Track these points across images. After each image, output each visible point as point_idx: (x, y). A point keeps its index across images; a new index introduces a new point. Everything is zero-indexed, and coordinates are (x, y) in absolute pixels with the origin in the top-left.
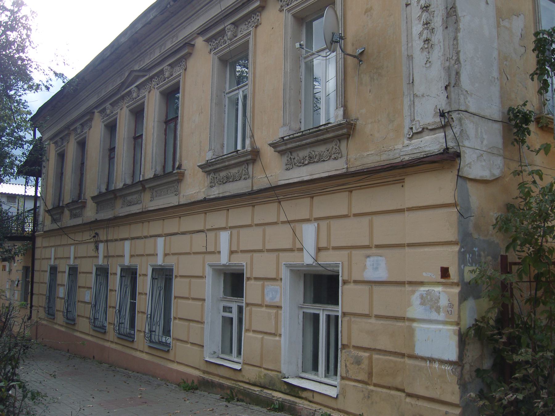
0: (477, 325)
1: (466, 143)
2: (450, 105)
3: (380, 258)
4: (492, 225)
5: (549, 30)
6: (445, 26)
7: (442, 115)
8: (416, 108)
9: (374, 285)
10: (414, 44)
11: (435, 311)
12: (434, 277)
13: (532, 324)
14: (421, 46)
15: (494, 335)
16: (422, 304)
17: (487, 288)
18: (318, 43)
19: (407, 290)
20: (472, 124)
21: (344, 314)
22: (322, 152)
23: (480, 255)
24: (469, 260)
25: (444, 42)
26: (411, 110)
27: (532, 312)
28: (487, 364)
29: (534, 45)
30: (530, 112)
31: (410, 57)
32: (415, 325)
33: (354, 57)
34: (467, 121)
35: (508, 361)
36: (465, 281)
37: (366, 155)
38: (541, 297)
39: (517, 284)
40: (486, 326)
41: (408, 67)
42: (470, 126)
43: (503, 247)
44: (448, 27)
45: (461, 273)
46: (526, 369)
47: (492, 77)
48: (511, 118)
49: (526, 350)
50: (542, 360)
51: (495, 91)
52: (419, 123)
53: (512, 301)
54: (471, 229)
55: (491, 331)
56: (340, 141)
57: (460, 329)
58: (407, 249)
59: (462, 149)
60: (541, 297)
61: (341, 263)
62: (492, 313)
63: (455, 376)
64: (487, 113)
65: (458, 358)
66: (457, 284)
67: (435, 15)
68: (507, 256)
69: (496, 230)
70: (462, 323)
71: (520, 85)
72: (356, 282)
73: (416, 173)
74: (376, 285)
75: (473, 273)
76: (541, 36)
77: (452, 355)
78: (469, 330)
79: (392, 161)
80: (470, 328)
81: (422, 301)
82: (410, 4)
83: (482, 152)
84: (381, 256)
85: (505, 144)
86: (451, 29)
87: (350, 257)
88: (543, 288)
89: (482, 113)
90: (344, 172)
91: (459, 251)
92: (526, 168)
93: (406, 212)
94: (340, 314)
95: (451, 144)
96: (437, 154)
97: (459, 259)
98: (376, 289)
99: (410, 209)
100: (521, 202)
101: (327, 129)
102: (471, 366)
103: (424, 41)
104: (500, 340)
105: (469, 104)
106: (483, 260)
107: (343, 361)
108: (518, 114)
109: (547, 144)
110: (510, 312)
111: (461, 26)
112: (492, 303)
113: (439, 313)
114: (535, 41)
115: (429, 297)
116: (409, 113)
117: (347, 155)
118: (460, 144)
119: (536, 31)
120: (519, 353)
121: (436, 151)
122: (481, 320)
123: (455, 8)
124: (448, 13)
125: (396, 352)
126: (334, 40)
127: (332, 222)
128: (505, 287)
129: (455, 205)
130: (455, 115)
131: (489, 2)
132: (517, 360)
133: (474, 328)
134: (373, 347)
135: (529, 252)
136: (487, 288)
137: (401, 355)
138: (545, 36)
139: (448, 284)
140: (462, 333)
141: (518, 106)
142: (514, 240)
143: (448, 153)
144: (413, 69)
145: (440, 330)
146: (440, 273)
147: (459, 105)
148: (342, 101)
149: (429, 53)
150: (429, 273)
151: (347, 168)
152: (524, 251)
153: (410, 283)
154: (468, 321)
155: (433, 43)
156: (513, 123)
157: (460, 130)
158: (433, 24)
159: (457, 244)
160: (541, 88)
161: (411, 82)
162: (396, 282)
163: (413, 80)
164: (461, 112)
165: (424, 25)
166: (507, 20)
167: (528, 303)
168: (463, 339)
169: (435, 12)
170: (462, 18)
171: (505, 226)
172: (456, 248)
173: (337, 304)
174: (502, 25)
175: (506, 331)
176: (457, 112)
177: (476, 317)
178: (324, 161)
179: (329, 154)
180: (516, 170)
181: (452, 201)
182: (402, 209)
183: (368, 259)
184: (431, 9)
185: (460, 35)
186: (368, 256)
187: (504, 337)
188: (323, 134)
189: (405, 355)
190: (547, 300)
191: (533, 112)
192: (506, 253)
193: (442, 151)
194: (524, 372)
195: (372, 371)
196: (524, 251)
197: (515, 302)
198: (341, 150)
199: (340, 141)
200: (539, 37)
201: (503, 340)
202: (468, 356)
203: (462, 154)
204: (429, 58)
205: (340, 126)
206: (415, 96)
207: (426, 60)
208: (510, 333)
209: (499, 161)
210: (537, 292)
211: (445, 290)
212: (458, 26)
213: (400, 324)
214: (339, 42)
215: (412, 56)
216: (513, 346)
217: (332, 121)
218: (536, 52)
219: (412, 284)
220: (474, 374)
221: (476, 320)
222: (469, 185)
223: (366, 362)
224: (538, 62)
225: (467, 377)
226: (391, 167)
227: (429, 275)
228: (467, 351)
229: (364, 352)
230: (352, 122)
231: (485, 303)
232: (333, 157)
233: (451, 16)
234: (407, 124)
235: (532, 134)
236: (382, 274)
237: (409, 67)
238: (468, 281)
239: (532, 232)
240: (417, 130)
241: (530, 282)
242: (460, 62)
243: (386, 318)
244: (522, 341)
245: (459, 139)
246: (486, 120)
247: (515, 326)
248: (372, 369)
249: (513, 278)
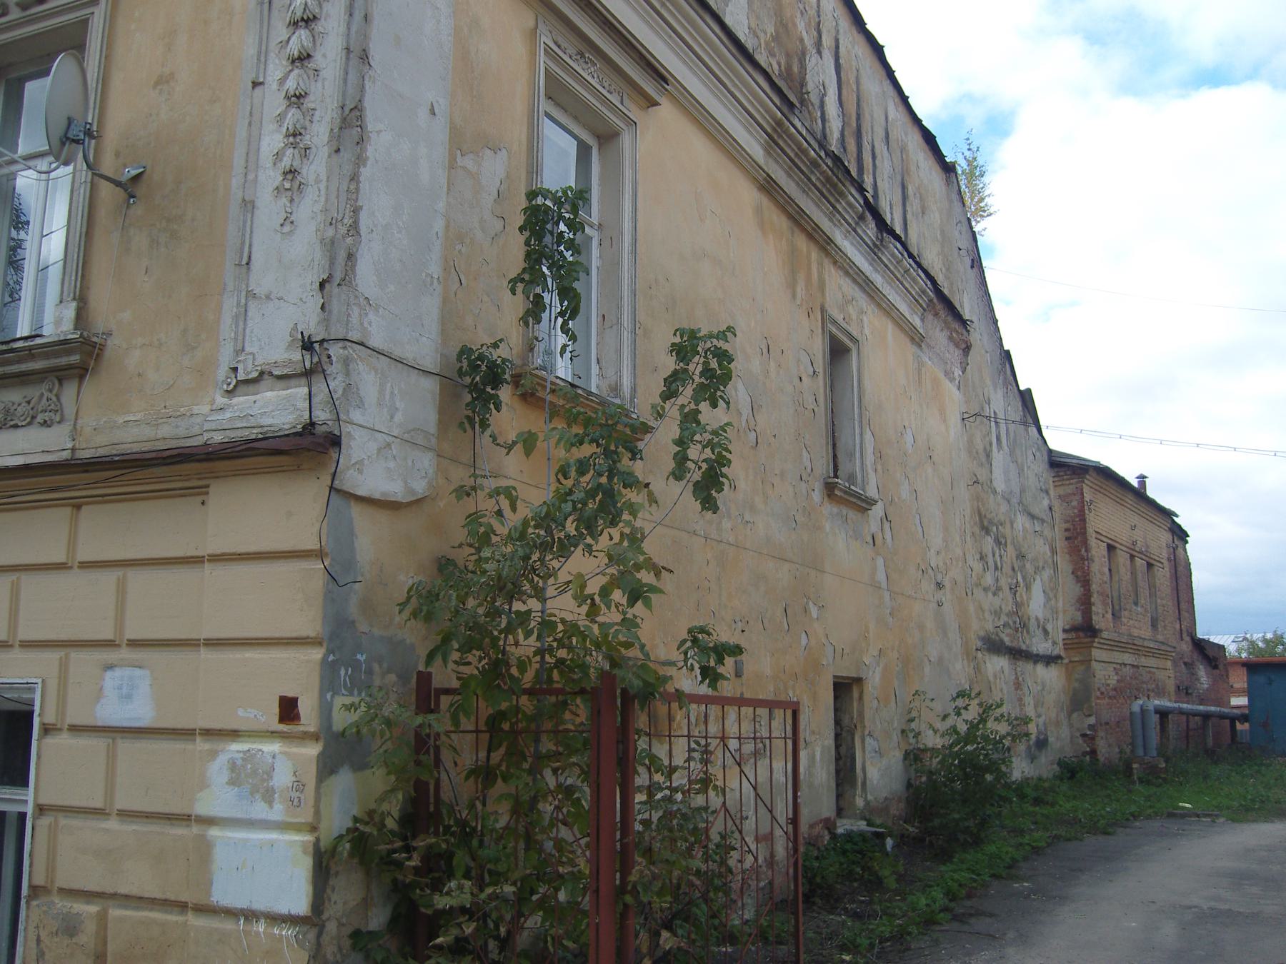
0: (357, 829)
1: (356, 416)
2: (326, 326)
3: (138, 672)
4: (398, 605)
5: (557, 191)
6: (335, 148)
7: (307, 345)
8: (250, 324)
9: (122, 738)
10: (262, 177)
11: (263, 799)
12: (263, 720)
13: (476, 826)
14: (277, 183)
15: (395, 851)
16: (232, 782)
17: (383, 744)
18: (31, 138)
19: (199, 748)
20: (373, 373)
22: (13, 404)
23: (370, 672)
24: (345, 680)
25: (328, 181)
26: (237, 326)
27: (478, 798)
28: (377, 919)
29: (523, 218)
30: (504, 361)
31: (249, 206)
32: (214, 832)
33: (118, 184)
34: (361, 367)
35: (423, 910)
36: (335, 728)
37: (121, 421)
38: (499, 765)
39: (449, 737)
40: (375, 833)
41: (241, 226)
42: (368, 379)
43: (423, 653)
44: (342, 150)
45: (326, 711)
46: (459, 925)
47: (428, 275)
48: (464, 369)
49: (459, 883)
50: (494, 904)
51: (431, 306)
52: (254, 359)
53: (437, 775)
54: (353, 610)
55: (388, 844)
56: (60, 381)
57: (318, 840)
58: (205, 653)
59: (346, 428)
60: (499, 765)
61: (39, 681)
62: (390, 802)
63: (303, 951)
64: (409, 353)
65: (310, 908)
66: (315, 737)
67: (316, 118)
68: (430, 674)
69: (407, 613)
70: (323, 826)
71: (485, 298)
72: (74, 729)
73: (236, 474)
74: (126, 738)
75: (352, 710)
76: (540, 200)
77: (298, 900)
78: (338, 843)
79: (183, 441)
80: (341, 837)
81: (234, 775)
82: (261, 83)
83: (390, 438)
84: (140, 667)
85: (443, 425)
86: (346, 155)
87: (64, 667)
88: (505, 744)
89: (397, 352)
90: (64, 458)
91: (324, 661)
92: (485, 482)
93: (207, 564)
94: (30, 809)
95: (321, 415)
96: (288, 435)
97: (322, 678)
98: (126, 747)
99: (217, 558)
100: (472, 555)
101: (30, 350)
102: (341, 925)
103: (285, 173)
104: (407, 863)
105: (370, 329)
106: (377, 682)
107: (31, 929)
108: (479, 363)
109: (529, 432)
110: (432, 800)
111: (370, 152)
112: (393, 778)
113: (270, 803)
114: (525, 210)
115: (249, 766)
116: (233, 335)
117: (76, 419)
118: (342, 417)
119: (530, 188)
120: (445, 890)
121: (286, 427)
122: (367, 819)
123: (361, 110)
124: (345, 119)
125: (166, 900)
126: (70, 135)
127: (25, 578)
128: (423, 744)
129: (320, 554)
130: (335, 350)
131: (436, 111)
132: (440, 906)
133: (350, 837)
134: (110, 890)
135: (480, 666)
136: (383, 744)
137: (178, 906)
138: (549, 203)
139: (294, 737)
140: (323, 850)
141: (482, 346)
142: (446, 640)
143: (314, 434)
144: (251, 232)
145: (272, 844)
146: (277, 710)
147: (347, 329)
148: (75, 286)
149: (292, 201)
150: (253, 710)
151: (73, 450)
152: (469, 663)
153: (208, 733)
154: (336, 821)
155: (302, 181)
156: (468, 380)
157: (344, 384)
158: (308, 137)
159: (320, 644)
160: (528, 313)
161: (244, 262)
162: (173, 729)
163: (250, 257)
164: (349, 344)
165: (287, 136)
166: (471, 156)
167: (472, 779)
168: (324, 865)
169: (317, 113)
170: (373, 136)
171: (425, 608)
172: (317, 654)
173: (24, 783)
174: (459, 164)
175: (420, 843)
176: (341, 344)
177: (355, 811)
178: (16, 426)
179: (31, 412)
180: (462, 484)
181: (313, 544)
182: (198, 557)
183: (109, 674)
184: (308, 103)
185: (365, 172)
186: (110, 667)
187: (415, 855)
188: (19, 362)
189: (187, 907)
190: (512, 771)
191: (510, 362)
192: (426, 668)
193: (299, 428)
194: (455, 932)
195: (106, 948)
196: (469, 663)
197: (444, 776)
198: (61, 404)
199: (60, 381)
200: (534, 203)
201: (412, 863)
202: (335, 903)
203: (344, 440)
204: (291, 213)
205: (62, 346)
206: (251, 295)
207: (284, 215)
208: (430, 847)
209: (426, 462)
210: (492, 754)
211: (287, 750)
212: (364, 150)
213: (179, 831)
214: (83, 143)
215: (253, 202)
216: (437, 875)
217: (46, 331)
218: (527, 234)
219: (212, 735)
220: (347, 943)
221: (356, 820)
222: (356, 510)
223: (90, 927)
224: (528, 255)
225: (330, 951)
226: (179, 455)
227: (252, 716)
228: (333, 890)
229: (88, 903)
230: (95, 339)
231: (378, 780)
232: (40, 419)
233: (350, 126)
234: (225, 357)
235: (504, 408)
236: (141, 711)
237: (244, 226)
238: (341, 729)
239: (482, 622)
240: (248, 373)
241: (477, 731)
242: (358, 233)
243: (147, 817)
244: (454, 863)
245: (341, 403)
246: (407, 367)
247: (441, 829)
248: (105, 943)
249: (439, 723)
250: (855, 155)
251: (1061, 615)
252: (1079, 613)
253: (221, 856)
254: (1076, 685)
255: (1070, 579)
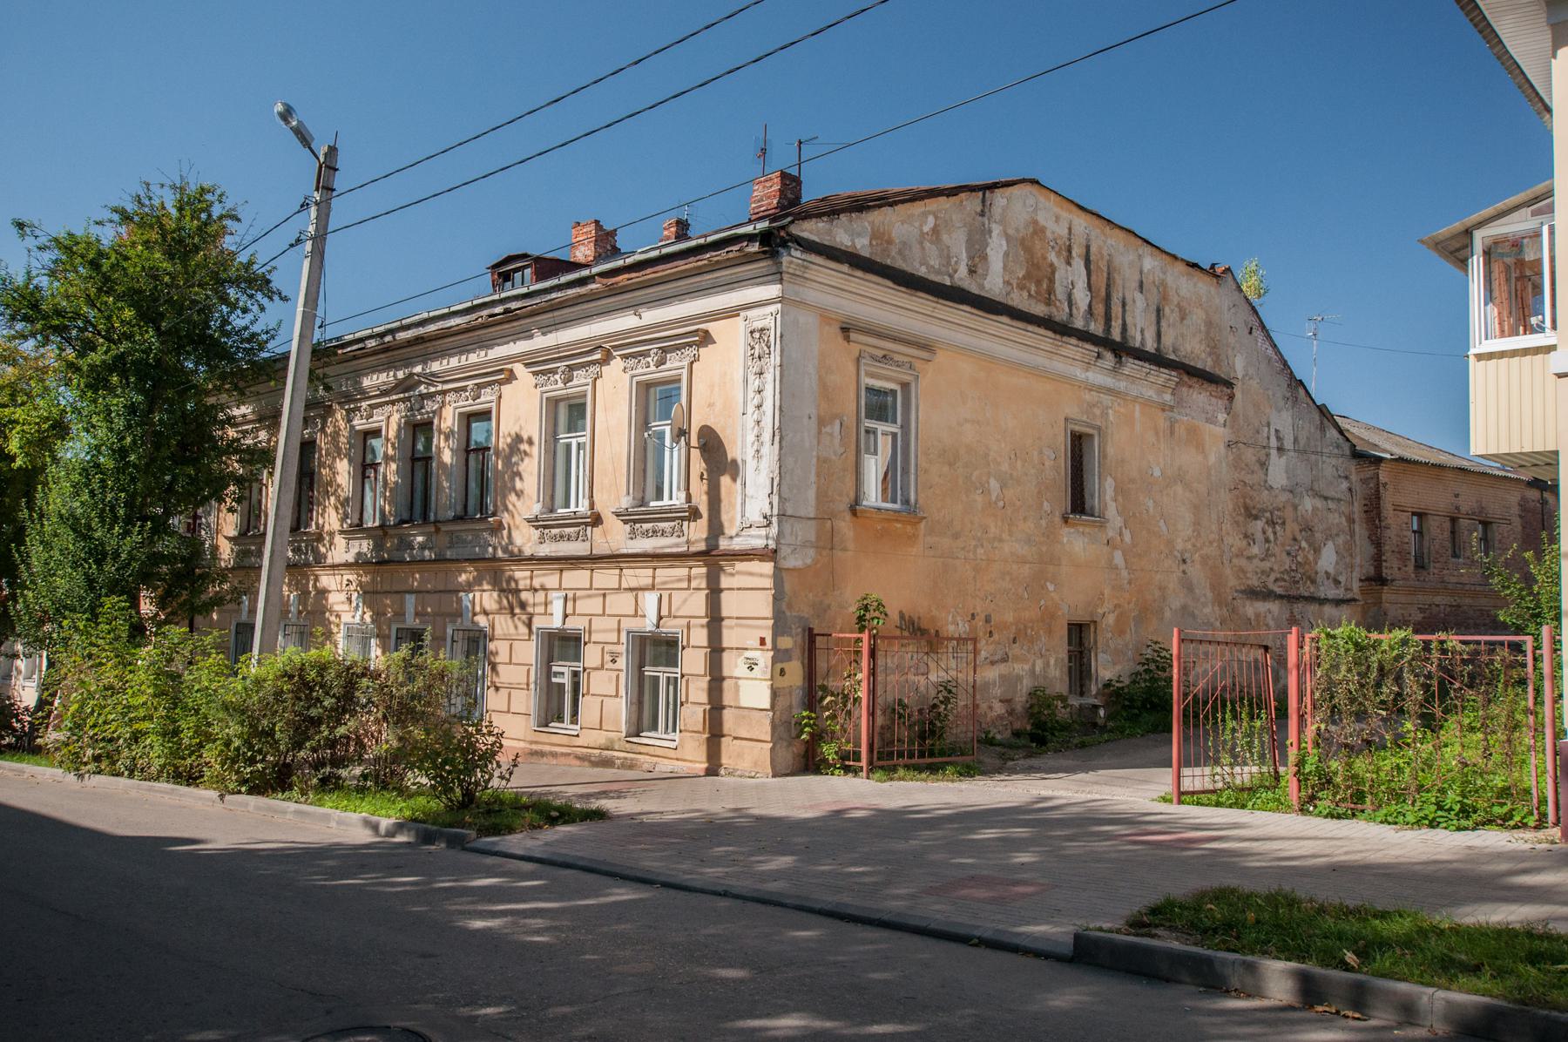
21: (683, 676)
94: (679, 676)
250: (1103, 314)
251: (1357, 569)
252: (1372, 568)
253: (704, 758)
254: (1370, 620)
255: (1367, 543)
